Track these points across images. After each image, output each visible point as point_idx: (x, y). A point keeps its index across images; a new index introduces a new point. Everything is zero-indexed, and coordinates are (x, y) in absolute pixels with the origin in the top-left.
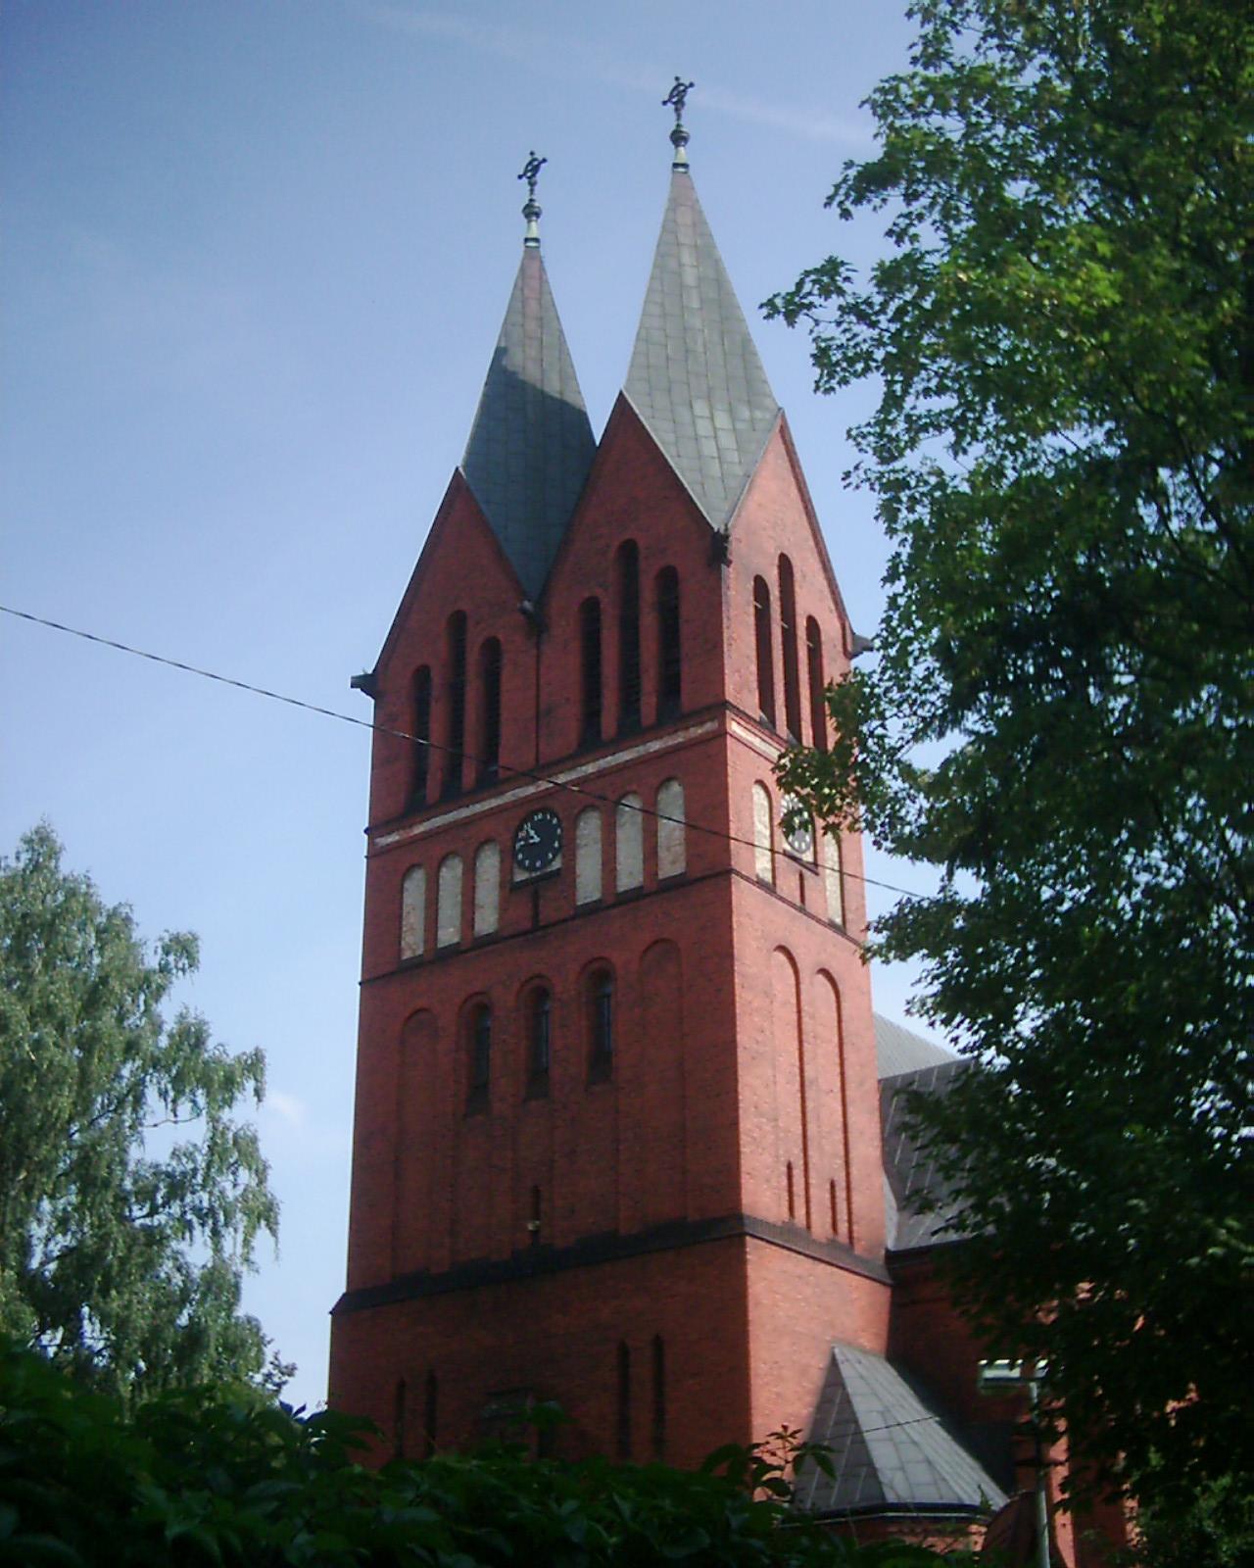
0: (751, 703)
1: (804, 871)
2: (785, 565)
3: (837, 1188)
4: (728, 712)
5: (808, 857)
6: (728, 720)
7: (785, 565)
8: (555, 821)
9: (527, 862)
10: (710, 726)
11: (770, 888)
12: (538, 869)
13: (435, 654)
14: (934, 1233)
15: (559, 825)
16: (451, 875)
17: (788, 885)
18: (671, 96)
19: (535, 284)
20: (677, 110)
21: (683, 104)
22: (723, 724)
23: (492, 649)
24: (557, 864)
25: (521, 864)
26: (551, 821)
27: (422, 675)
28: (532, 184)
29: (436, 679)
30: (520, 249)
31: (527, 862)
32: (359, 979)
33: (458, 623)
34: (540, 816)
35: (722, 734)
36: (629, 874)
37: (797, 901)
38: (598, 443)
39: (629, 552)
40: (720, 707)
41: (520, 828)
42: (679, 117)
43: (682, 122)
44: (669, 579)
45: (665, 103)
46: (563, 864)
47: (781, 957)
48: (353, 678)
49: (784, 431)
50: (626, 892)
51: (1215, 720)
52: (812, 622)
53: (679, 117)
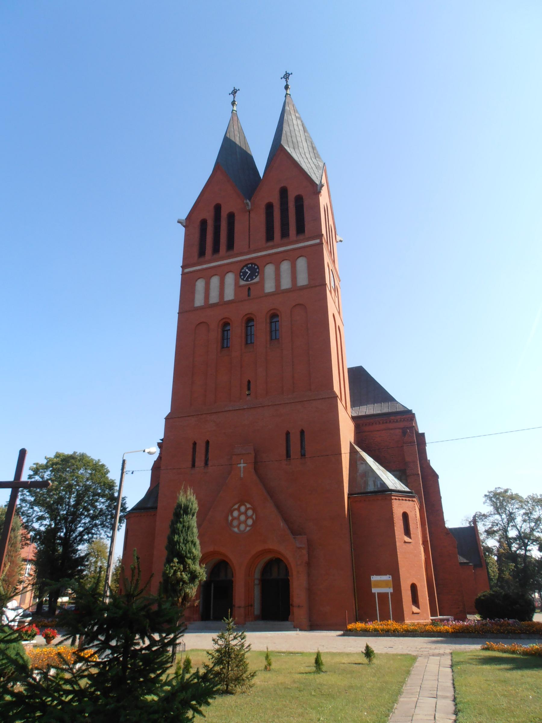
8: (256, 267)
9: (253, 266)
12: (249, 281)
20: (286, 80)
23: (231, 217)
25: (243, 279)
27: (204, 223)
31: (253, 266)
33: (218, 208)
38: (261, 174)
41: (243, 269)
42: (287, 82)
43: (288, 83)
44: (299, 199)
50: (283, 290)
51: (99, 639)
53: (287, 82)
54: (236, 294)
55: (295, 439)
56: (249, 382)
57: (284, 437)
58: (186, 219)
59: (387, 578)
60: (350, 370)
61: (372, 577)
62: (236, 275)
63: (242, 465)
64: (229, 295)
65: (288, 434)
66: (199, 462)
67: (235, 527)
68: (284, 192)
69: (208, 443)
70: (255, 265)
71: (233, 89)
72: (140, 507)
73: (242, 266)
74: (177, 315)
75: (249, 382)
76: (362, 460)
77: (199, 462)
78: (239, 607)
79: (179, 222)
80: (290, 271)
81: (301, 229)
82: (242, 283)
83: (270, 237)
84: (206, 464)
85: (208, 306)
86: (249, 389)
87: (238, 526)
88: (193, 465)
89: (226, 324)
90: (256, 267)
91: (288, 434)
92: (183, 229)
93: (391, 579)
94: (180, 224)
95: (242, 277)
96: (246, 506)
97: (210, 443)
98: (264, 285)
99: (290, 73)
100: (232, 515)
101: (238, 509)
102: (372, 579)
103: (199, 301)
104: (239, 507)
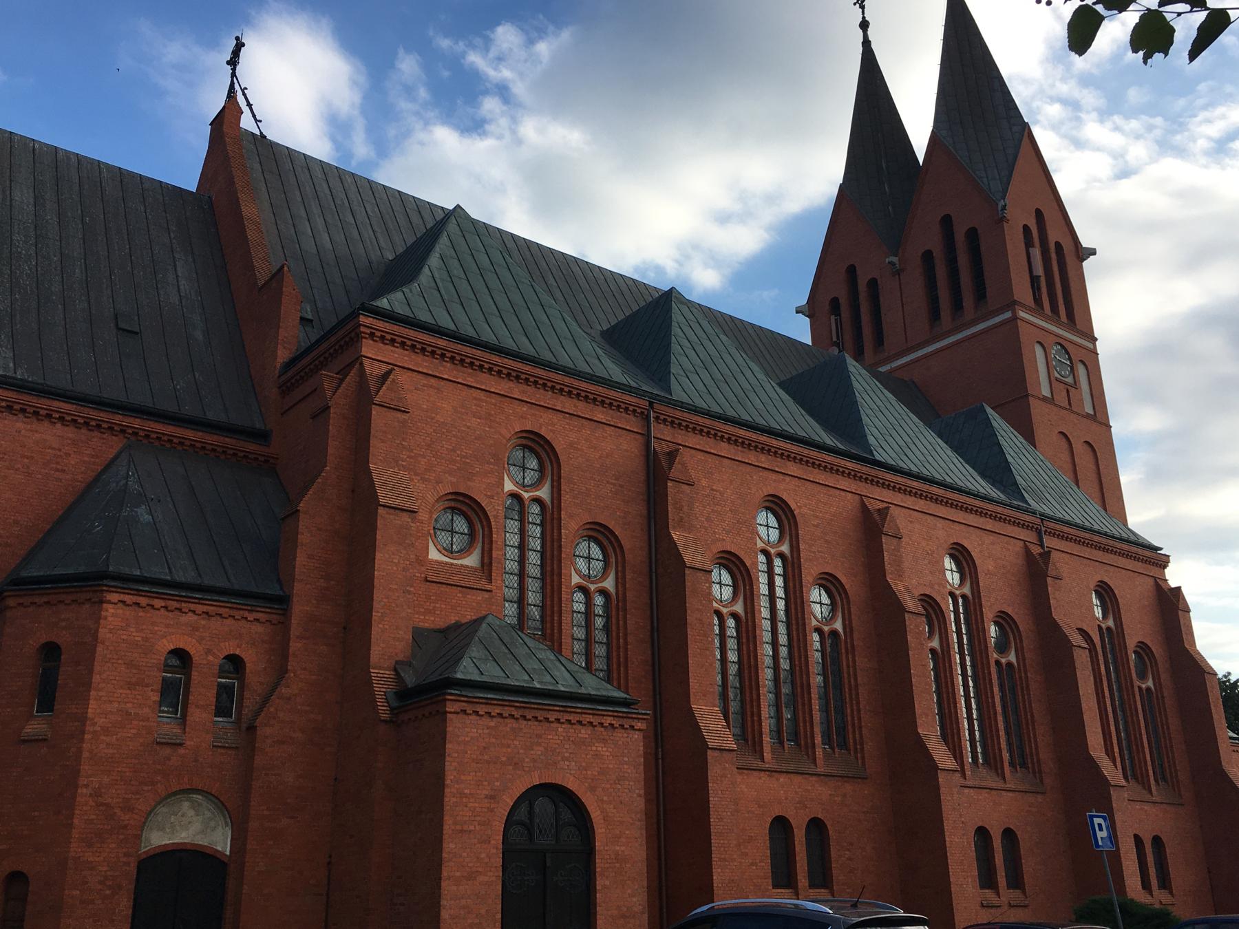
0: (1028, 298)
1: (1070, 388)
2: (1039, 214)
4: (1016, 306)
5: (1070, 380)
6: (1017, 311)
7: (1039, 214)
10: (1008, 315)
11: (1050, 401)
14: (1174, 790)
17: (1061, 399)
22: (1014, 313)
23: (873, 284)
29: (843, 302)
35: (1015, 318)
37: (1066, 404)
39: (947, 221)
40: (1012, 305)
44: (972, 234)
52: (1058, 245)
79: (797, 312)
92: (808, 320)
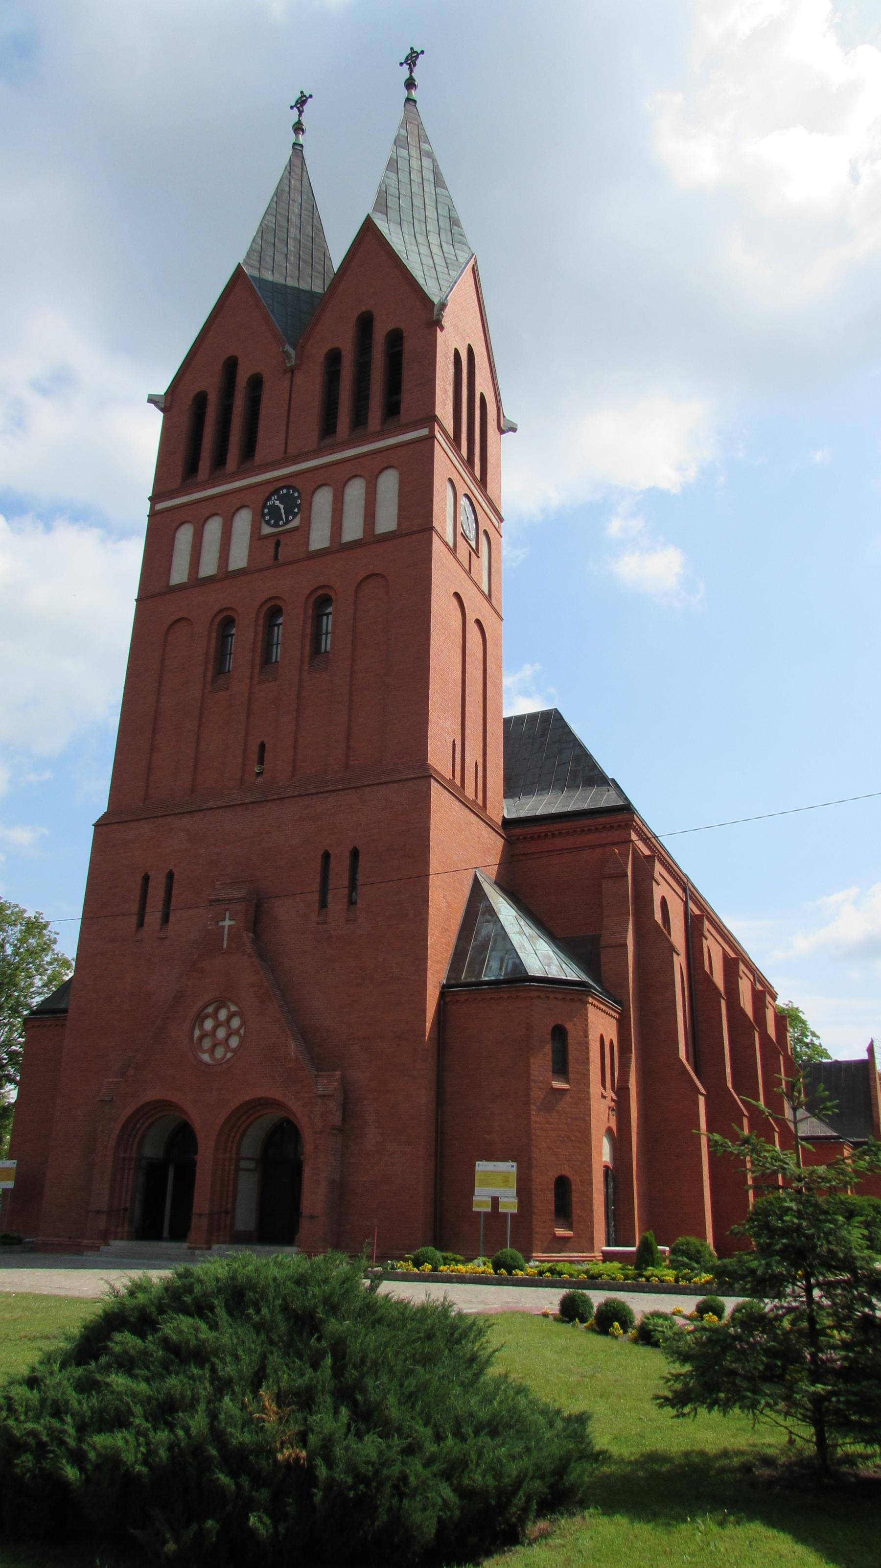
3: (151, 883)
8: (296, 494)
13: (211, 384)
15: (299, 497)
16: (213, 528)
18: (407, 59)
19: (299, 171)
21: (415, 65)
23: (256, 383)
24: (296, 523)
25: (268, 523)
26: (293, 494)
27: (201, 400)
28: (301, 113)
30: (289, 151)
32: (136, 598)
33: (231, 366)
34: (285, 491)
36: (353, 530)
40: (431, 419)
41: (269, 499)
44: (395, 339)
45: (401, 64)
46: (301, 522)
47: (455, 602)
48: (149, 395)
49: (475, 270)
52: (482, 396)
53: (411, 71)
54: (251, 557)
55: (340, 868)
56: (262, 746)
57: (317, 865)
58: (165, 394)
59: (509, 1168)
60: (507, 721)
61: (477, 1163)
62: (254, 514)
63: (227, 923)
64: (239, 559)
65: (326, 856)
66: (153, 917)
67: (205, 1052)
68: (365, 323)
69: (170, 876)
70: (295, 489)
71: (300, 95)
72: (43, 1010)
73: (267, 494)
74: (135, 603)
75: (262, 746)
76: (490, 915)
77: (153, 917)
78: (200, 1215)
80: (363, 503)
81: (392, 409)
82: (266, 530)
83: (328, 428)
84: (166, 919)
85: (196, 582)
86: (261, 761)
87: (212, 1051)
88: (141, 923)
89: (229, 622)
90: (296, 494)
91: (326, 856)
92: (161, 415)
93: (515, 1169)
94: (152, 405)
95: (267, 518)
96: (229, 1009)
97: (175, 877)
98: (309, 534)
99: (419, 52)
100: (201, 1026)
101: (215, 1015)
102: (477, 1168)
103: (179, 574)
104: (217, 1010)
